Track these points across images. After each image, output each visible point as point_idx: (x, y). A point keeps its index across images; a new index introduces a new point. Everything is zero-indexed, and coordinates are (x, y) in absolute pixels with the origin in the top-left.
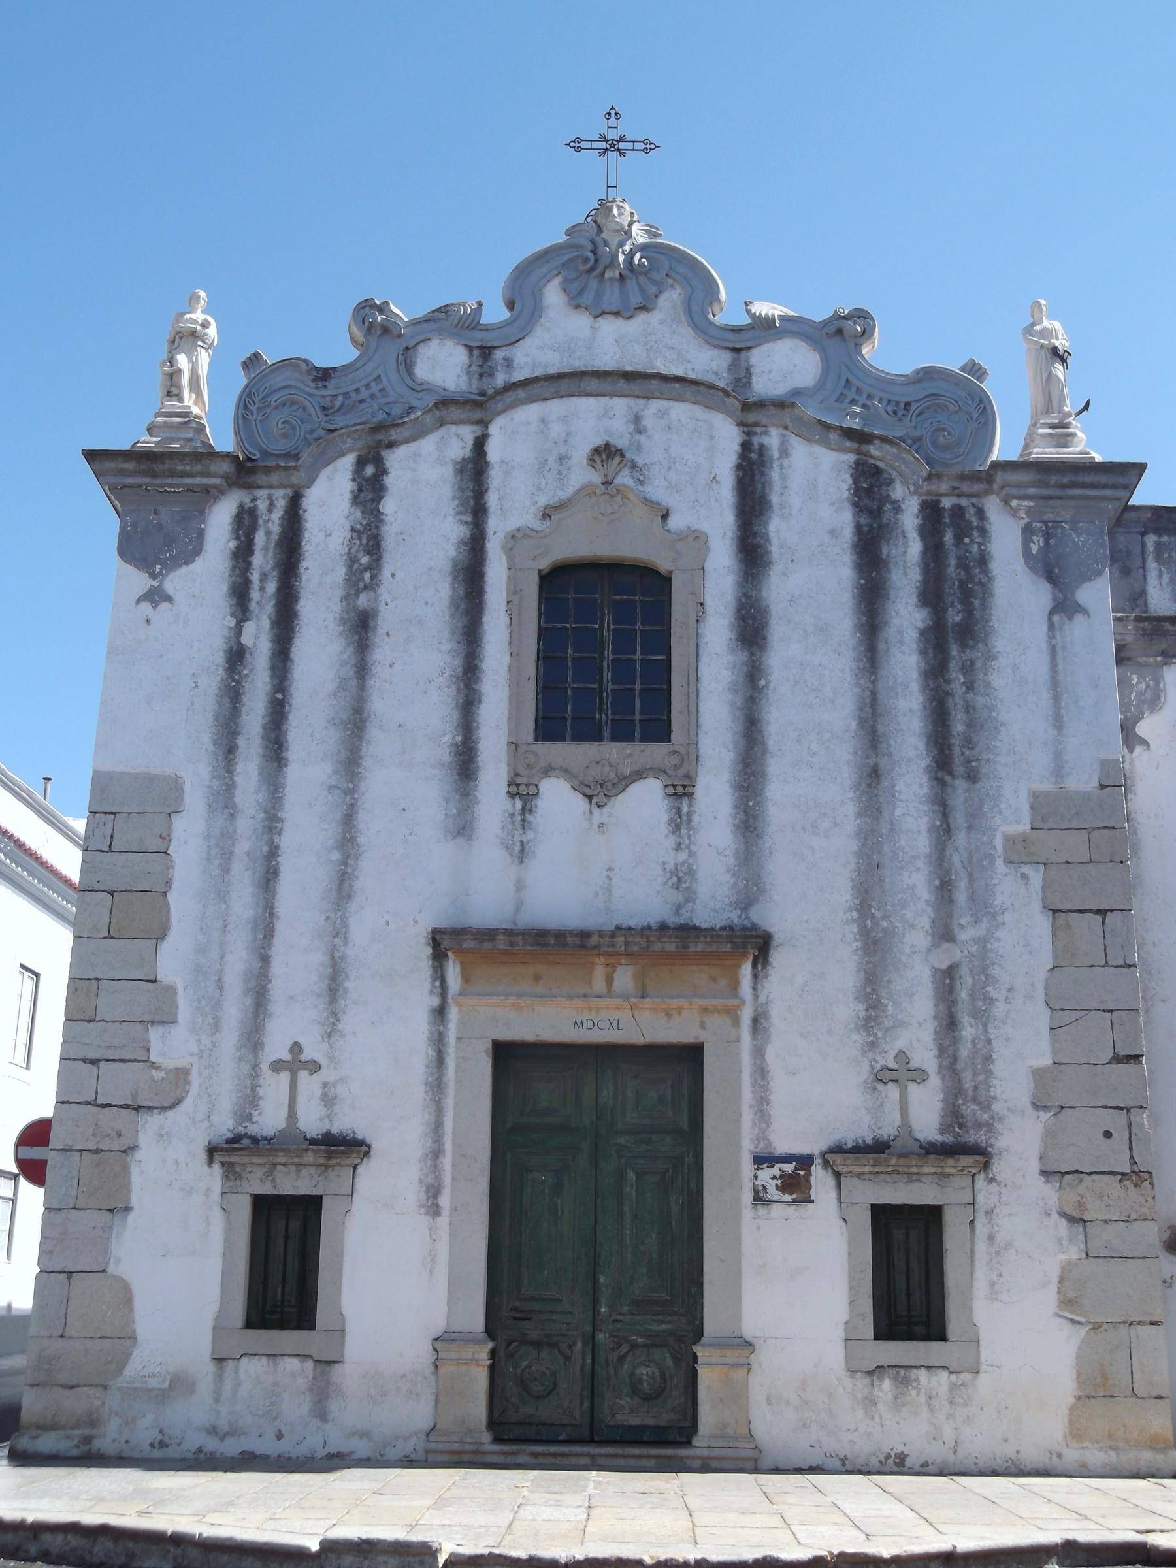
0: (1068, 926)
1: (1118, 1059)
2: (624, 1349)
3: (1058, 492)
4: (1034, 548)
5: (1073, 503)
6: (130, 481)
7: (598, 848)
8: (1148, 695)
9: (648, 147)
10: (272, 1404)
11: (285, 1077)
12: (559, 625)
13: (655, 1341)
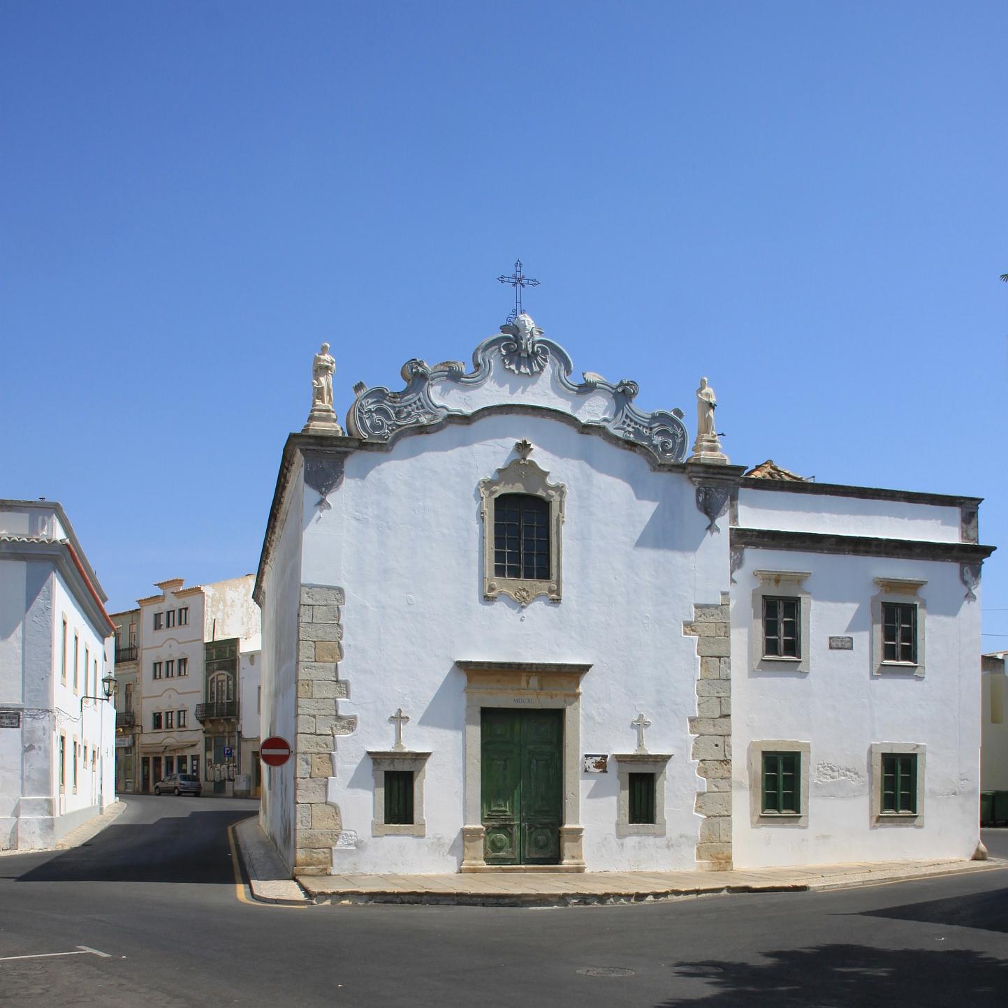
0: (706, 662)
2: (533, 829)
3: (712, 476)
4: (701, 499)
5: (717, 480)
6: (311, 447)
7: (523, 633)
8: (738, 562)
9: (535, 283)
10: (427, 846)
12: (501, 523)
13: (544, 826)
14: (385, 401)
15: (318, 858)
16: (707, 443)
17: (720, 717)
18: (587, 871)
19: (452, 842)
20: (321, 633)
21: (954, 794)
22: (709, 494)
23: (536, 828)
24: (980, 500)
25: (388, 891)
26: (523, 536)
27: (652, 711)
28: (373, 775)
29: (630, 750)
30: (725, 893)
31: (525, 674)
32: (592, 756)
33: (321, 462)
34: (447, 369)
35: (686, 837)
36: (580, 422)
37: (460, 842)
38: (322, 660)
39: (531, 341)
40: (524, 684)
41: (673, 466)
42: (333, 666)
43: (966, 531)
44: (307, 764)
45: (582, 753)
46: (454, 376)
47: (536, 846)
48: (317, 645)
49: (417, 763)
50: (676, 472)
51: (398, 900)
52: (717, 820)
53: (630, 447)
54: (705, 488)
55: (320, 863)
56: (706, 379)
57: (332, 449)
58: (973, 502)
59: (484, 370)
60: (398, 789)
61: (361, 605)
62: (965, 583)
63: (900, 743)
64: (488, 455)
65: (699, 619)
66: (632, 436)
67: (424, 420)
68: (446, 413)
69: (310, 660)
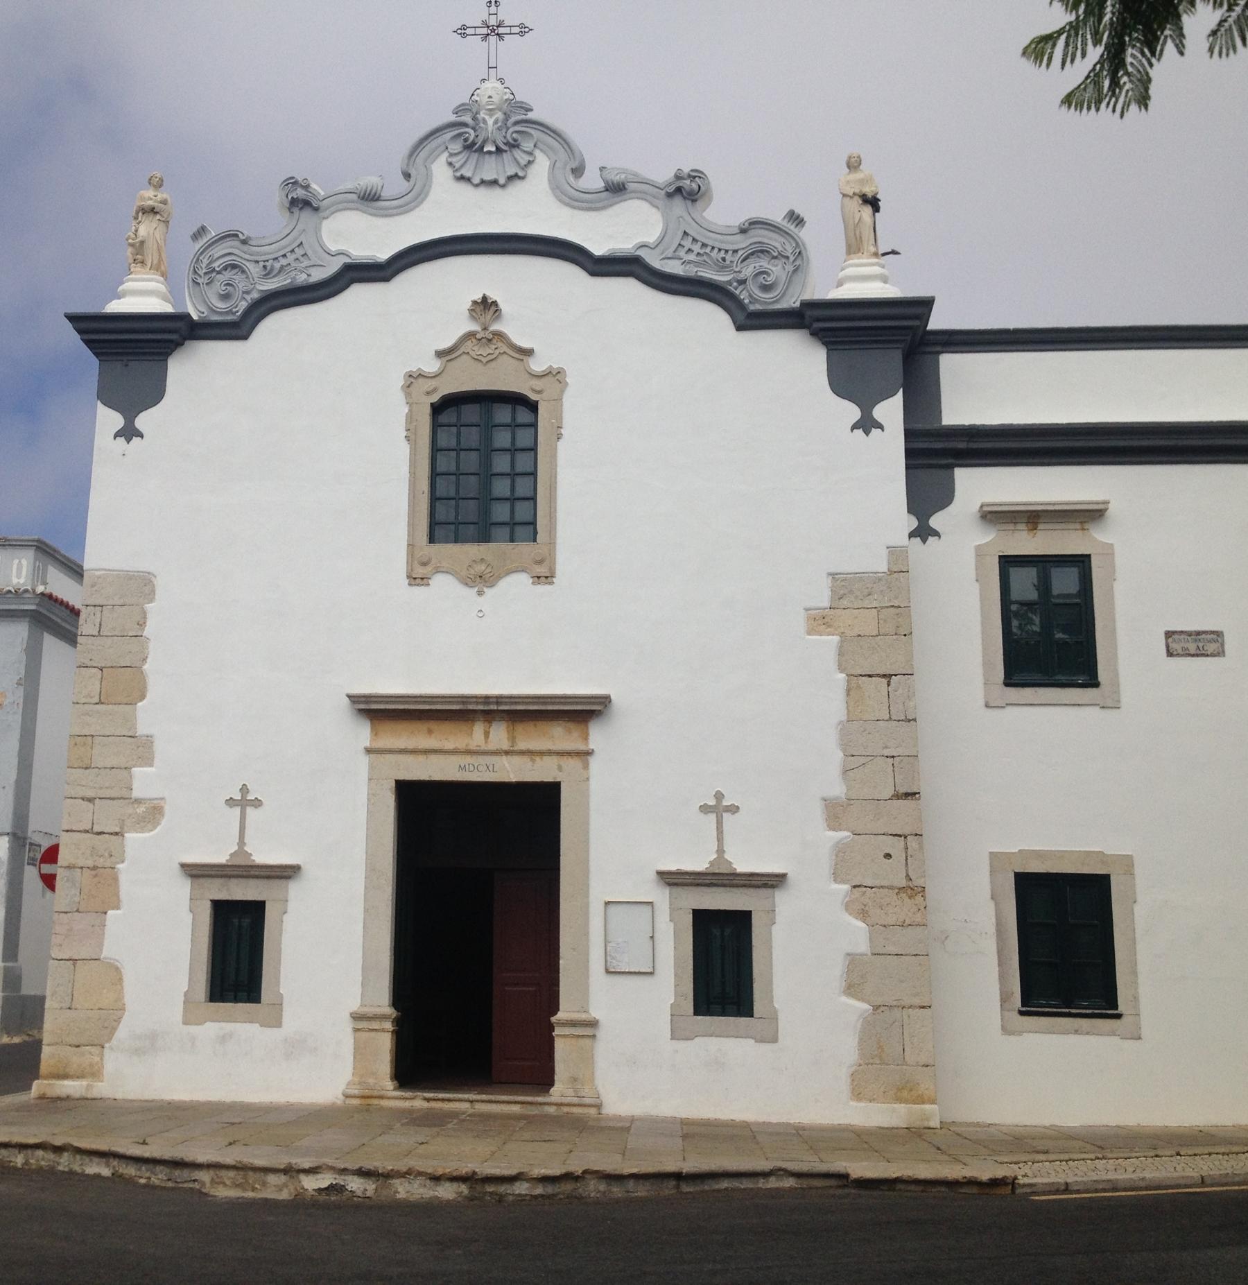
0: (859, 687)
1: (898, 796)
7: (480, 637)
9: (523, 30)
11: (237, 810)
26: (482, 466)
29: (698, 863)
46: (369, 198)
60: (236, 957)
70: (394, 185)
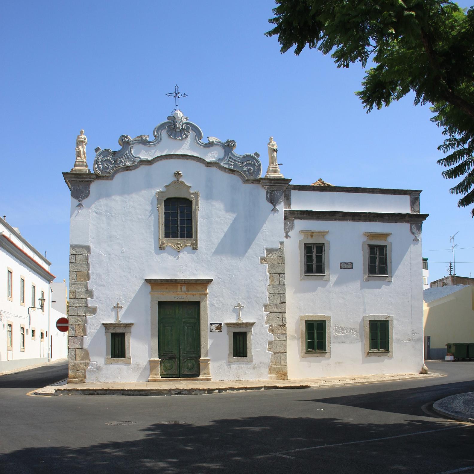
2: (186, 360)
3: (274, 184)
4: (268, 196)
5: (276, 187)
7: (179, 265)
8: (291, 226)
9: (185, 95)
14: (110, 156)
15: (79, 375)
16: (272, 169)
17: (280, 304)
18: (212, 380)
19: (144, 367)
20: (79, 267)
21: (409, 340)
22: (273, 194)
23: (187, 360)
24: (421, 191)
25: (91, 389)
26: (178, 219)
27: (244, 301)
28: (105, 335)
29: (234, 321)
30: (263, 389)
31: (180, 285)
32: (214, 324)
33: (79, 186)
34: (140, 139)
35: (263, 363)
36: (206, 161)
37: (149, 367)
38: (80, 280)
39: (181, 123)
40: (179, 289)
41: (254, 180)
42: (85, 283)
43: (413, 207)
44: (73, 330)
45: (209, 322)
46: (143, 141)
47: (188, 368)
48: (78, 273)
49: (126, 328)
50: (256, 184)
51: (96, 393)
52: (279, 355)
53: (231, 172)
54: (271, 190)
55: (80, 377)
56: (272, 137)
57: (84, 179)
58: (417, 193)
59: (158, 139)
61: (99, 254)
62: (413, 233)
63: (379, 314)
64: (160, 180)
65: (268, 255)
66: (232, 167)
67: (128, 164)
68: (139, 160)
69: (74, 280)
70: (150, 138)
